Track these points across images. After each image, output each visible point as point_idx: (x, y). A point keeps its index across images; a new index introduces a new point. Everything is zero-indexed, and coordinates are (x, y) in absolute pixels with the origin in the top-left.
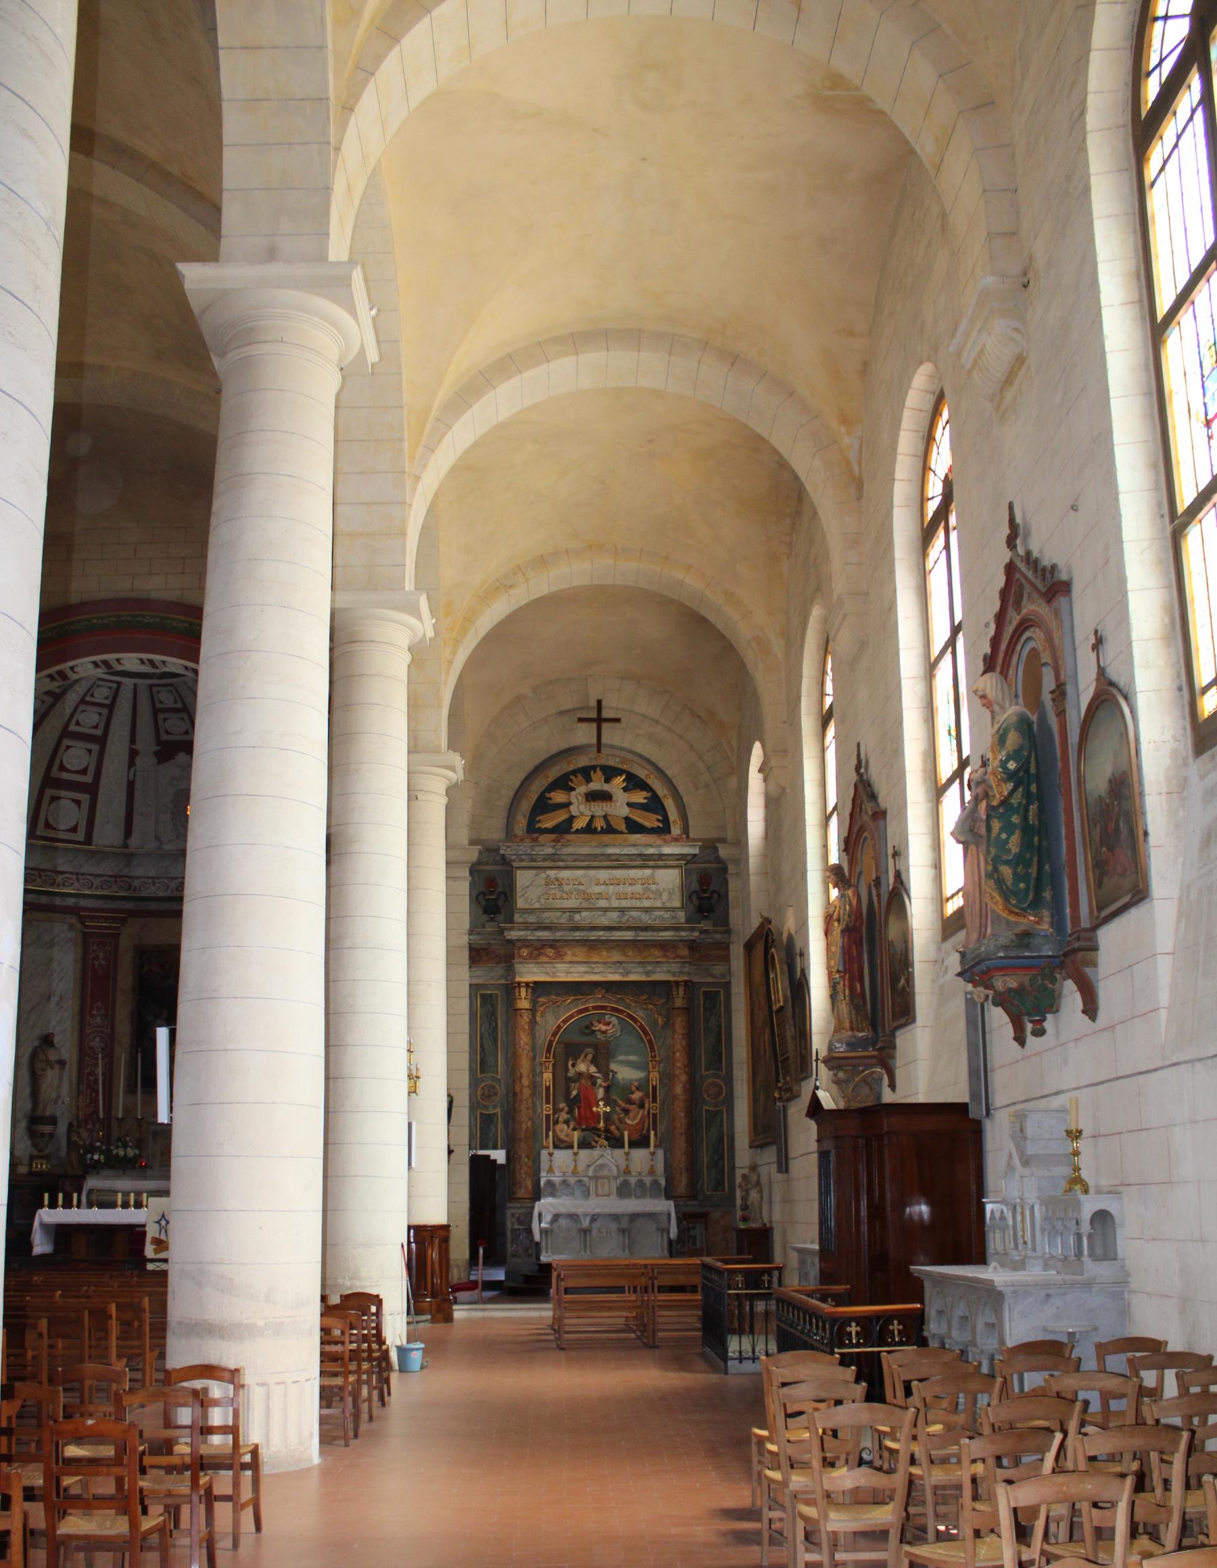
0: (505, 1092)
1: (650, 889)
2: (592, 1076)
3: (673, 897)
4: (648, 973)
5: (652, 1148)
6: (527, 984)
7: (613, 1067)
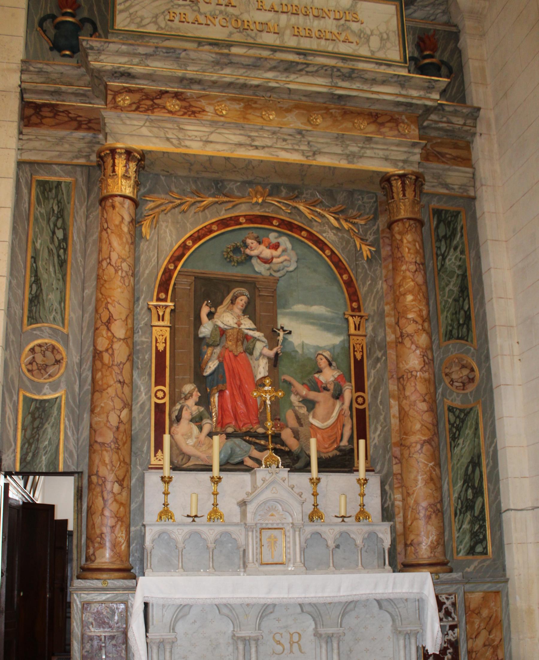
0: (76, 359)
1: (348, 28)
2: (246, 337)
3: (388, 45)
4: (351, 157)
5: (362, 474)
6: (129, 153)
7: (283, 321)
